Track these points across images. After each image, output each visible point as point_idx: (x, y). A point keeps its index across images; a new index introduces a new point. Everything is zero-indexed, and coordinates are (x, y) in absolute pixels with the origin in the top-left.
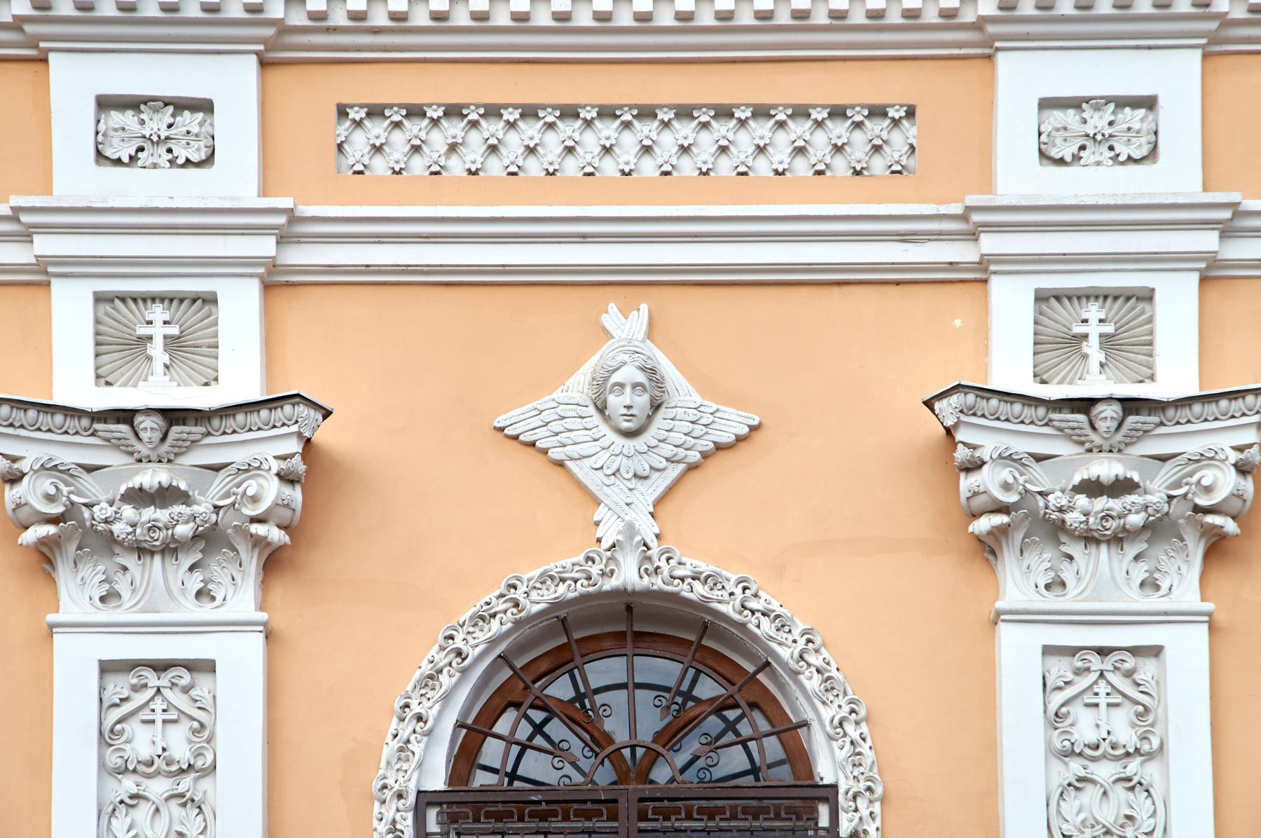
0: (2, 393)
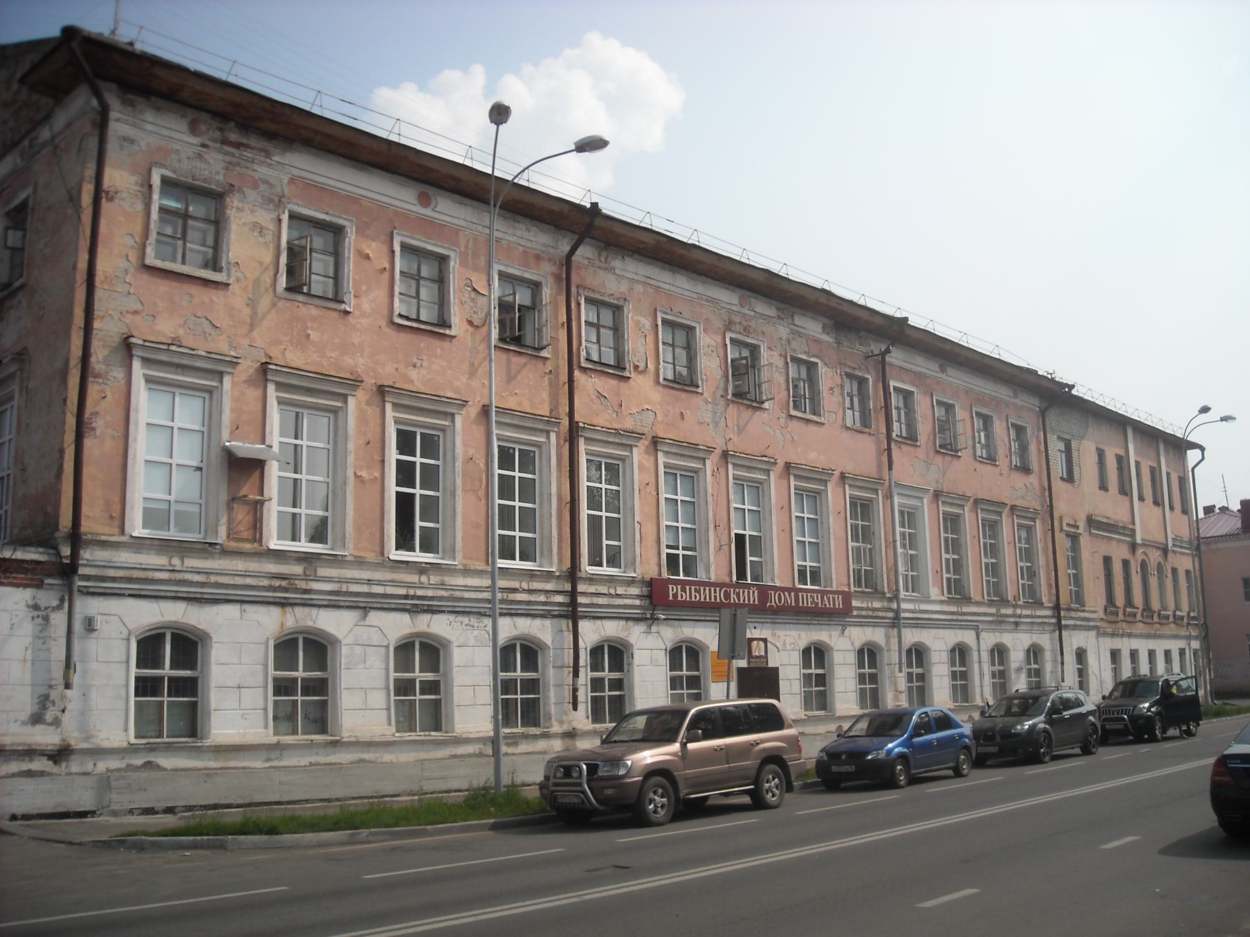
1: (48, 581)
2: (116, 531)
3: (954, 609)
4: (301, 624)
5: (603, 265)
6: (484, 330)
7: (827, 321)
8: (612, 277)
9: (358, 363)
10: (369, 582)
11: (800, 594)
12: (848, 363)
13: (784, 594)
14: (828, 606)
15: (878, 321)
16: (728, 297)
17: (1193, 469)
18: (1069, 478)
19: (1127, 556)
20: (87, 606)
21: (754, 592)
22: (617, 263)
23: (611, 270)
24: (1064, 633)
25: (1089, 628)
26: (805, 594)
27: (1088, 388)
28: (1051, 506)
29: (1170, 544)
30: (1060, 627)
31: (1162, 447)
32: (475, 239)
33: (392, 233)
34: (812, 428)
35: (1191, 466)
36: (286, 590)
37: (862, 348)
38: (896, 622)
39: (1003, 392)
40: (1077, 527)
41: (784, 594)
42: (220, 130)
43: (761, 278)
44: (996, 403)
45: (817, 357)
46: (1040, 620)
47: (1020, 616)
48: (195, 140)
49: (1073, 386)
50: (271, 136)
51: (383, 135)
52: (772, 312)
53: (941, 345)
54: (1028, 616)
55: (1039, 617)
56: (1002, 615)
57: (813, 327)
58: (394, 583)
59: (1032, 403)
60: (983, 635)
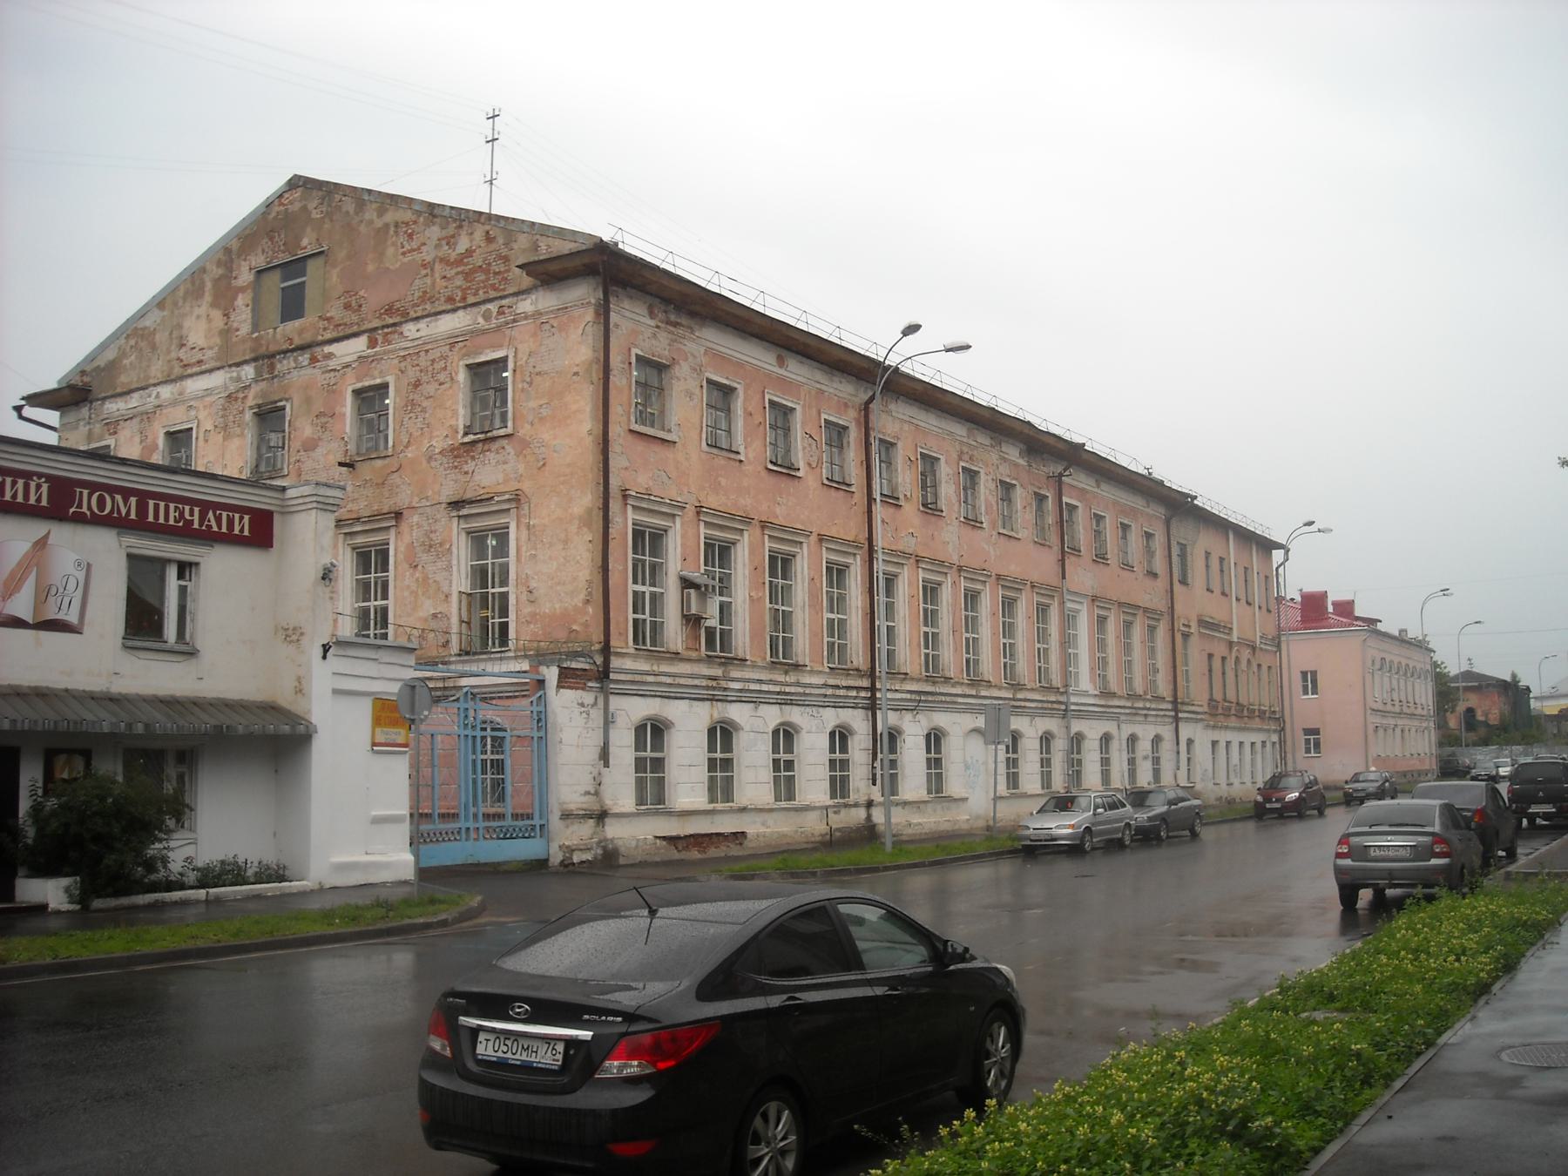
1: (590, 684)
2: (623, 645)
3: (1102, 702)
4: (722, 715)
5: (883, 409)
6: (819, 469)
7: (1022, 446)
8: (890, 419)
9: (746, 504)
10: (760, 681)
11: (151, 503)
12: (1036, 483)
13: (113, 499)
14: (215, 528)
15: (1061, 446)
16: (959, 430)
17: (1277, 569)
18: (1184, 582)
19: (1225, 652)
20: (616, 702)
21: (39, 487)
22: (892, 406)
23: (889, 413)
24: (1180, 725)
25: (1197, 721)
26: (162, 504)
27: (1211, 498)
28: (1172, 607)
29: (1258, 643)
30: (1177, 720)
31: (1231, 536)
32: (810, 392)
33: (763, 392)
34: (1013, 542)
35: (1275, 566)
36: (714, 688)
37: (1045, 469)
38: (1065, 714)
39: (1137, 502)
40: (1189, 626)
41: (113, 499)
42: (666, 312)
43: (987, 414)
44: (1133, 512)
45: (1016, 479)
46: (1162, 713)
47: (1149, 709)
48: (652, 323)
49: (1196, 497)
50: (693, 314)
51: (747, 303)
52: (987, 441)
53: (1102, 464)
54: (1154, 710)
55: (1162, 710)
56: (1135, 708)
57: (1013, 452)
58: (771, 682)
59: (1159, 511)
60: (1123, 726)
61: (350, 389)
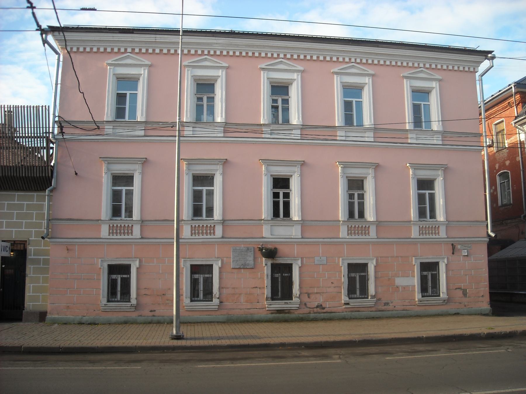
0: (524, 294)
21: (43, 140)
61: (509, 171)
